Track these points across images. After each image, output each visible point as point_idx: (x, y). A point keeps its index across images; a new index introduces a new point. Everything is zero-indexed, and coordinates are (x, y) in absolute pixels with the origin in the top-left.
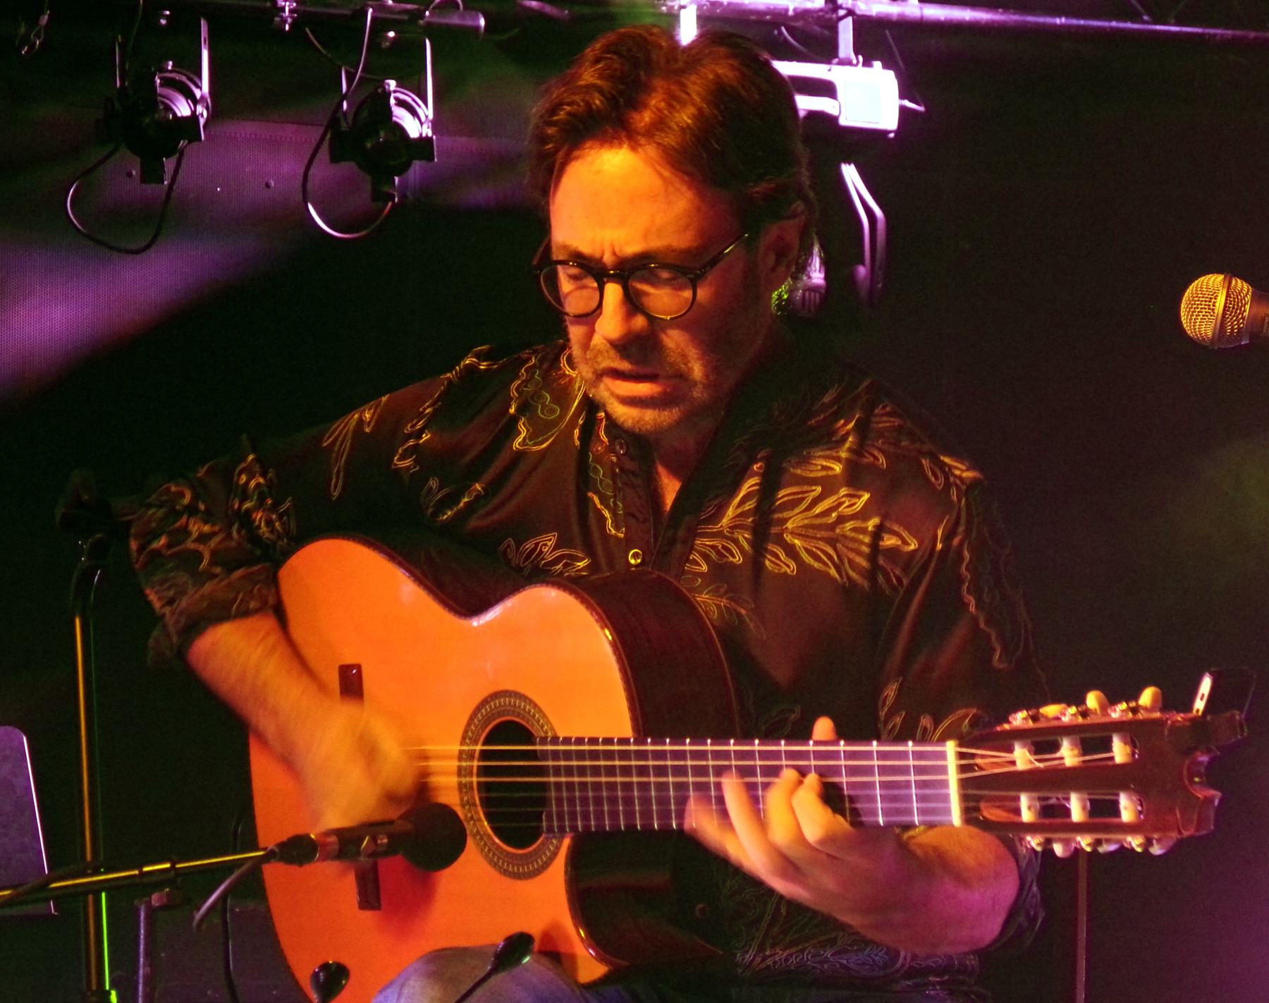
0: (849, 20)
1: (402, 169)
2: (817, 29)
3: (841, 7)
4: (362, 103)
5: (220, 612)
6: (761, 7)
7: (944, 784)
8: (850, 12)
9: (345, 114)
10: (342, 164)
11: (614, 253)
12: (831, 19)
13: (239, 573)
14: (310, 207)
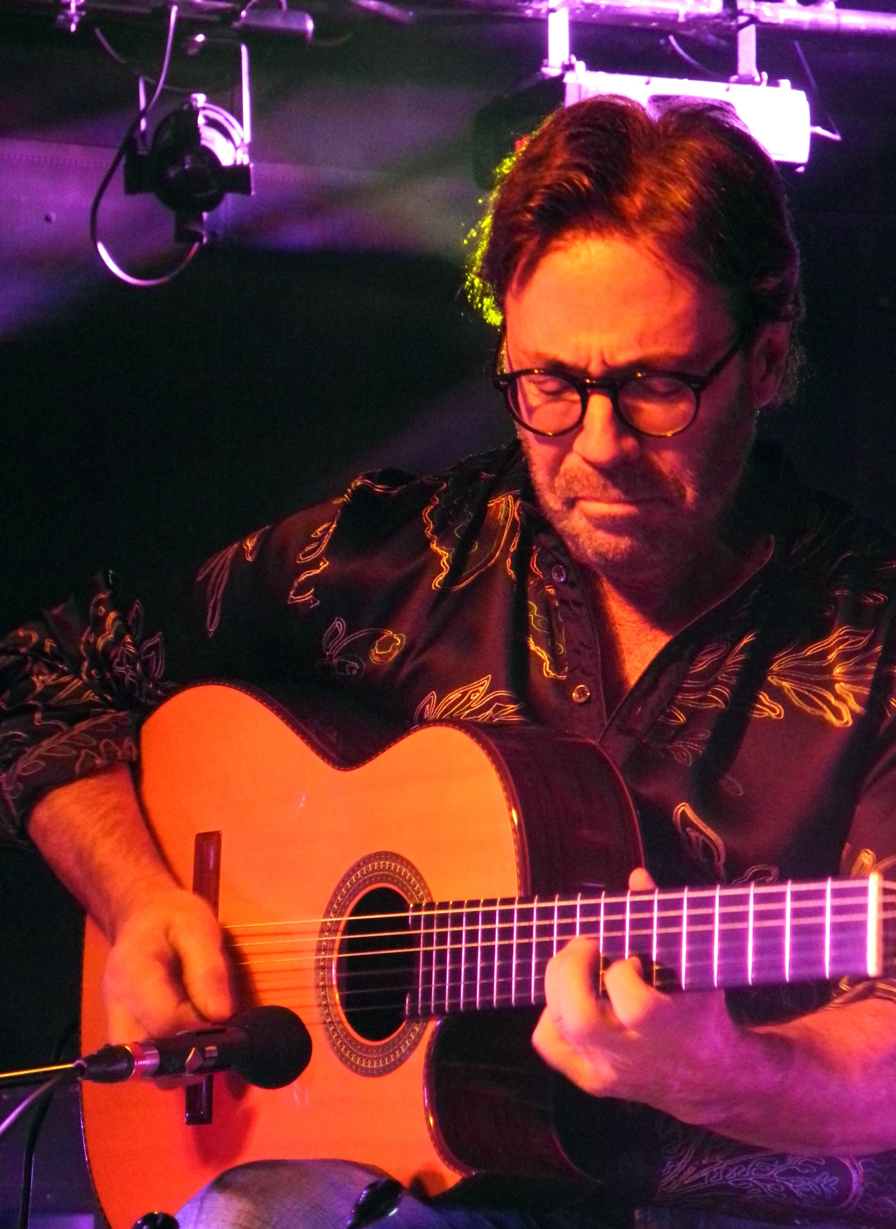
0: (752, 29)
1: (212, 204)
2: (711, 37)
3: (741, 13)
4: (166, 120)
5: (63, 774)
6: (646, 12)
8: (753, 19)
9: (144, 134)
10: (140, 196)
11: (604, 362)
12: (729, 28)
13: (83, 725)
14: (101, 248)
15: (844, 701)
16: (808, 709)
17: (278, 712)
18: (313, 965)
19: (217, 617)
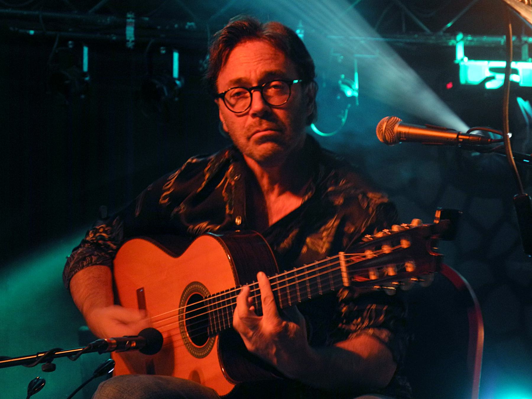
17: (154, 243)
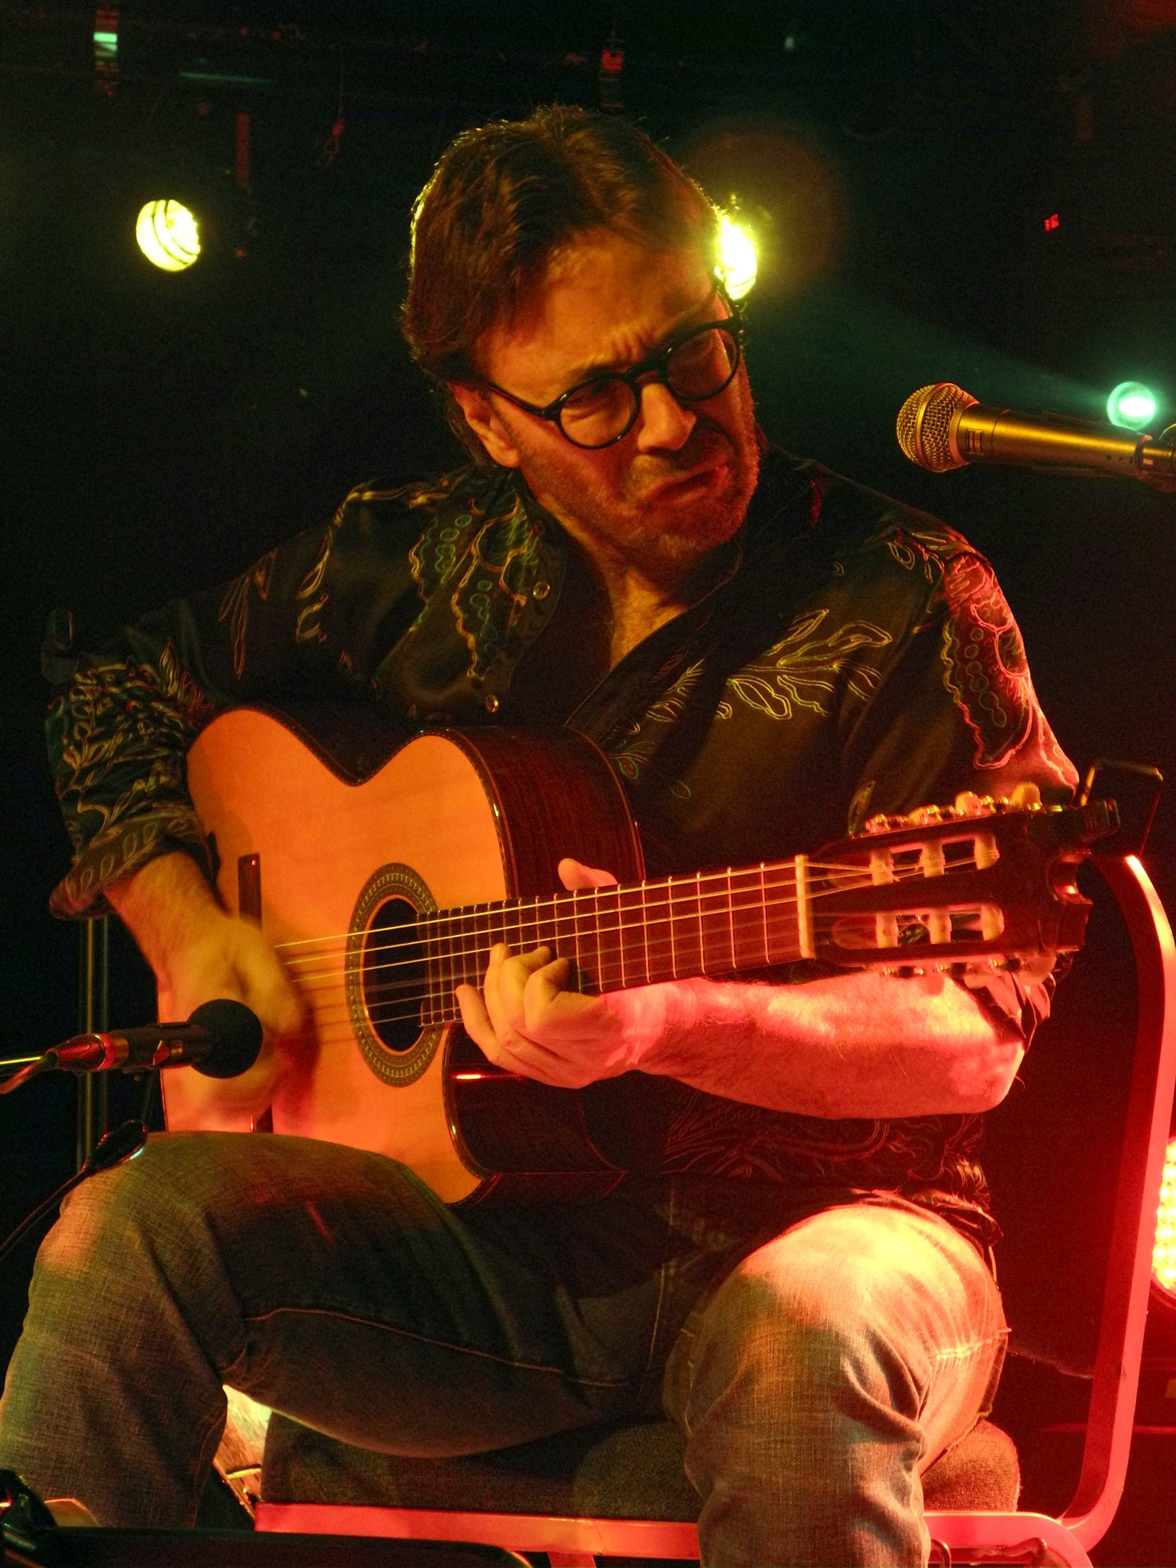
7: (793, 907)
15: (787, 695)
16: (751, 703)
17: (297, 732)
18: (343, 982)
19: (242, 660)
